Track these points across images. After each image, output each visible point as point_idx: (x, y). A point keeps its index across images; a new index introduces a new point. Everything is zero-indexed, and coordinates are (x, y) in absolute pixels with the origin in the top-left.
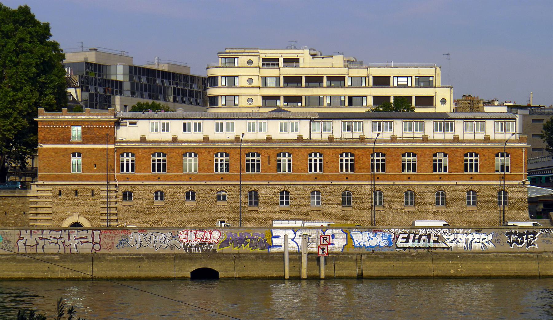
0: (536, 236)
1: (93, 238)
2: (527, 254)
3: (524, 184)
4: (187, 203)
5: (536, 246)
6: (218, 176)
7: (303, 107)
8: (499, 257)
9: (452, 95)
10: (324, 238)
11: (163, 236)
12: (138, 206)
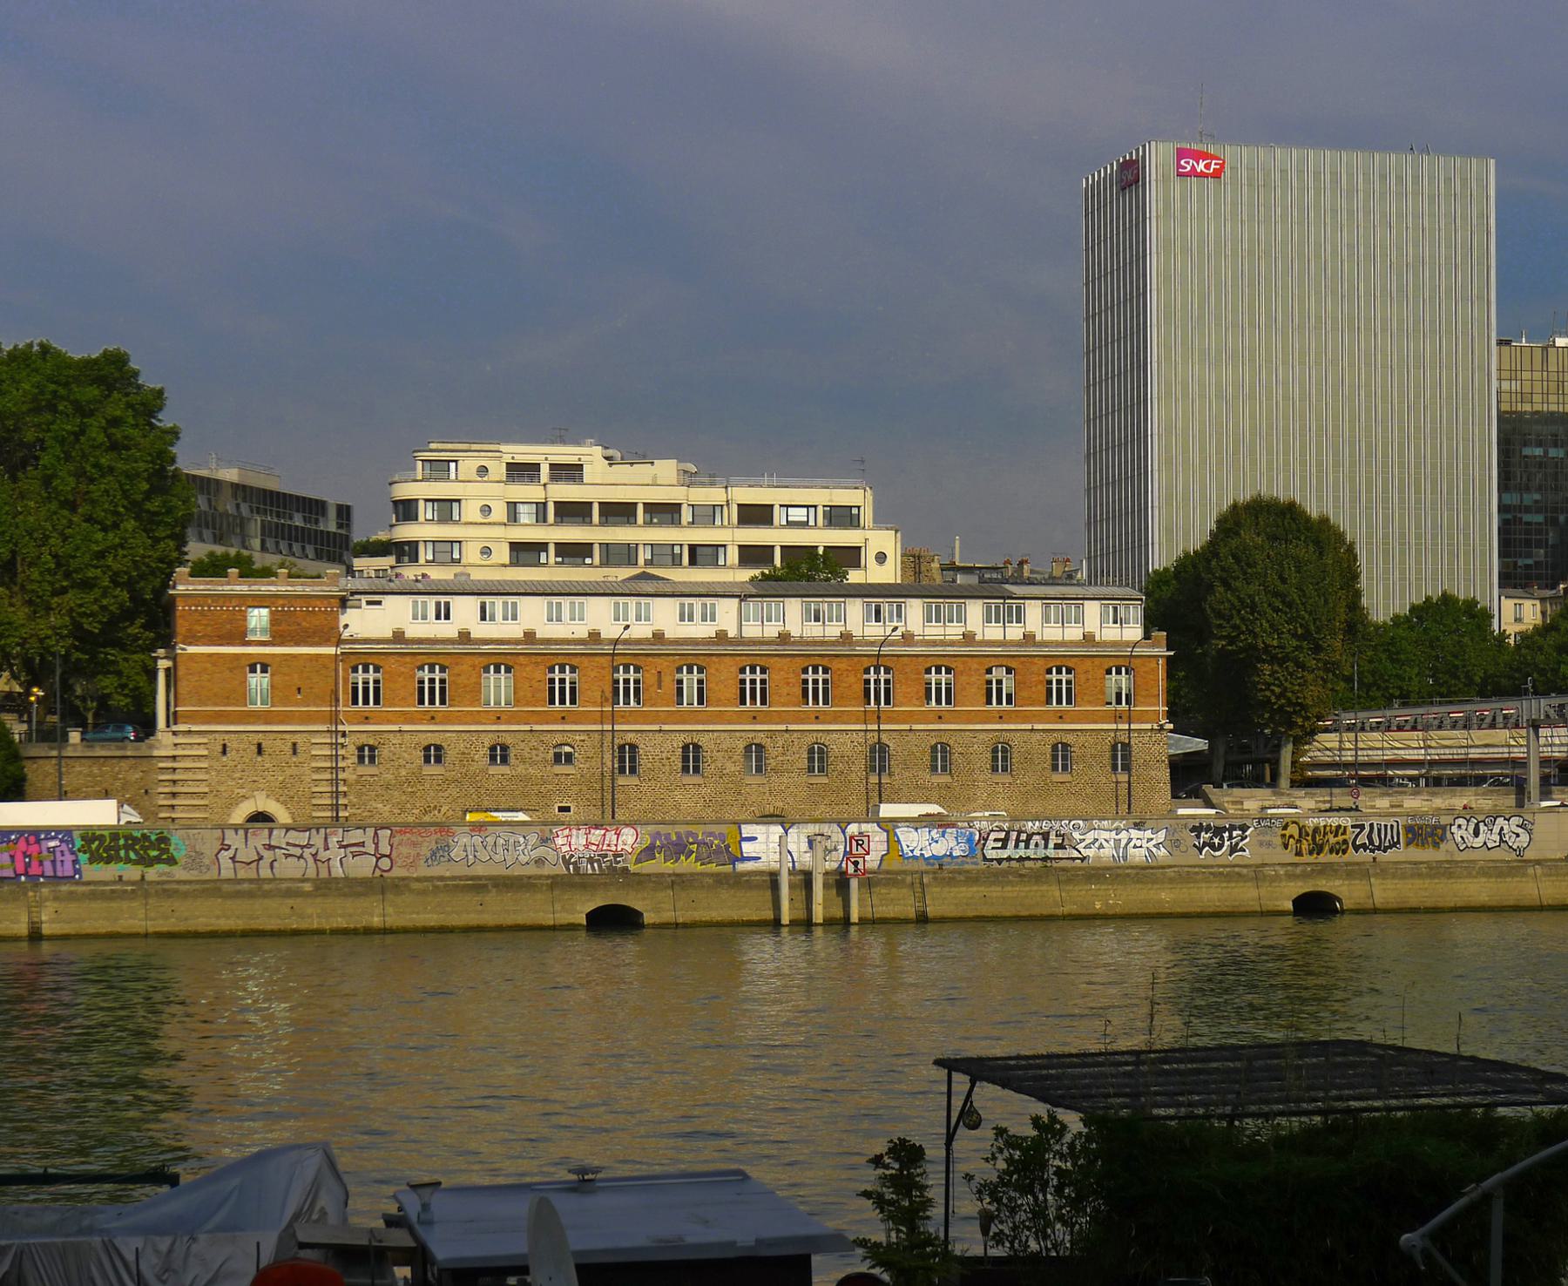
0: (1247, 833)
1: (377, 845)
2: (1237, 869)
3: (1161, 728)
4: (493, 770)
5: (1247, 853)
6: (555, 714)
7: (597, 567)
8: (1185, 876)
9: (899, 545)
10: (857, 841)
11: (522, 840)
12: (389, 777)
